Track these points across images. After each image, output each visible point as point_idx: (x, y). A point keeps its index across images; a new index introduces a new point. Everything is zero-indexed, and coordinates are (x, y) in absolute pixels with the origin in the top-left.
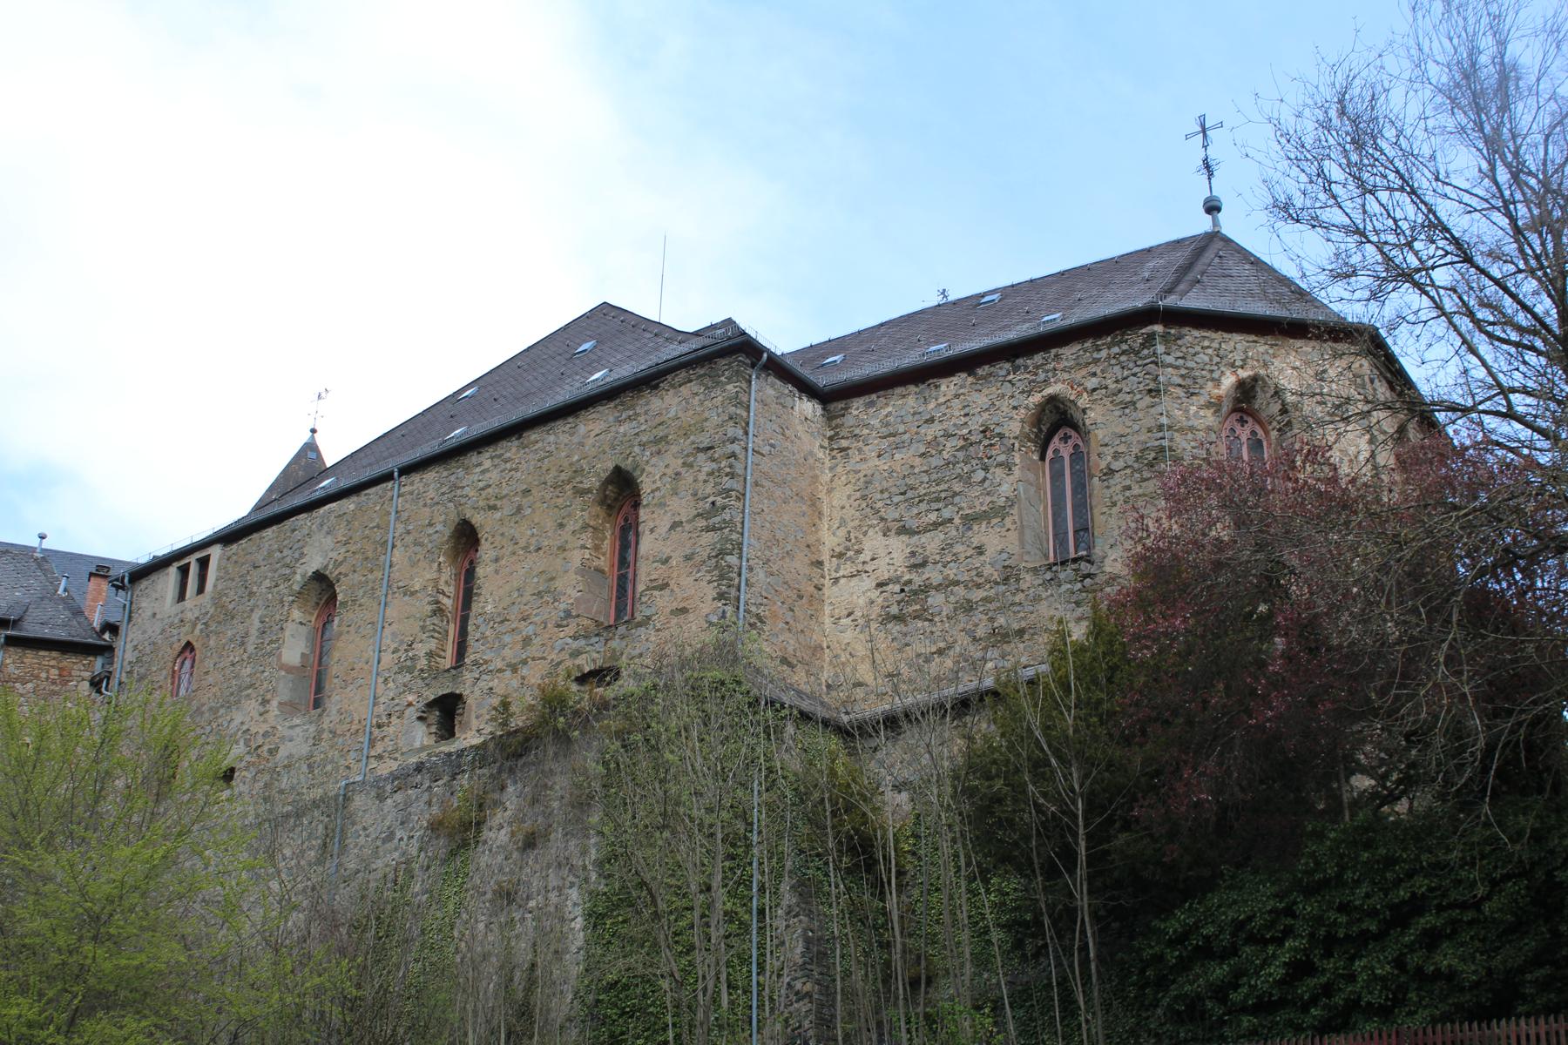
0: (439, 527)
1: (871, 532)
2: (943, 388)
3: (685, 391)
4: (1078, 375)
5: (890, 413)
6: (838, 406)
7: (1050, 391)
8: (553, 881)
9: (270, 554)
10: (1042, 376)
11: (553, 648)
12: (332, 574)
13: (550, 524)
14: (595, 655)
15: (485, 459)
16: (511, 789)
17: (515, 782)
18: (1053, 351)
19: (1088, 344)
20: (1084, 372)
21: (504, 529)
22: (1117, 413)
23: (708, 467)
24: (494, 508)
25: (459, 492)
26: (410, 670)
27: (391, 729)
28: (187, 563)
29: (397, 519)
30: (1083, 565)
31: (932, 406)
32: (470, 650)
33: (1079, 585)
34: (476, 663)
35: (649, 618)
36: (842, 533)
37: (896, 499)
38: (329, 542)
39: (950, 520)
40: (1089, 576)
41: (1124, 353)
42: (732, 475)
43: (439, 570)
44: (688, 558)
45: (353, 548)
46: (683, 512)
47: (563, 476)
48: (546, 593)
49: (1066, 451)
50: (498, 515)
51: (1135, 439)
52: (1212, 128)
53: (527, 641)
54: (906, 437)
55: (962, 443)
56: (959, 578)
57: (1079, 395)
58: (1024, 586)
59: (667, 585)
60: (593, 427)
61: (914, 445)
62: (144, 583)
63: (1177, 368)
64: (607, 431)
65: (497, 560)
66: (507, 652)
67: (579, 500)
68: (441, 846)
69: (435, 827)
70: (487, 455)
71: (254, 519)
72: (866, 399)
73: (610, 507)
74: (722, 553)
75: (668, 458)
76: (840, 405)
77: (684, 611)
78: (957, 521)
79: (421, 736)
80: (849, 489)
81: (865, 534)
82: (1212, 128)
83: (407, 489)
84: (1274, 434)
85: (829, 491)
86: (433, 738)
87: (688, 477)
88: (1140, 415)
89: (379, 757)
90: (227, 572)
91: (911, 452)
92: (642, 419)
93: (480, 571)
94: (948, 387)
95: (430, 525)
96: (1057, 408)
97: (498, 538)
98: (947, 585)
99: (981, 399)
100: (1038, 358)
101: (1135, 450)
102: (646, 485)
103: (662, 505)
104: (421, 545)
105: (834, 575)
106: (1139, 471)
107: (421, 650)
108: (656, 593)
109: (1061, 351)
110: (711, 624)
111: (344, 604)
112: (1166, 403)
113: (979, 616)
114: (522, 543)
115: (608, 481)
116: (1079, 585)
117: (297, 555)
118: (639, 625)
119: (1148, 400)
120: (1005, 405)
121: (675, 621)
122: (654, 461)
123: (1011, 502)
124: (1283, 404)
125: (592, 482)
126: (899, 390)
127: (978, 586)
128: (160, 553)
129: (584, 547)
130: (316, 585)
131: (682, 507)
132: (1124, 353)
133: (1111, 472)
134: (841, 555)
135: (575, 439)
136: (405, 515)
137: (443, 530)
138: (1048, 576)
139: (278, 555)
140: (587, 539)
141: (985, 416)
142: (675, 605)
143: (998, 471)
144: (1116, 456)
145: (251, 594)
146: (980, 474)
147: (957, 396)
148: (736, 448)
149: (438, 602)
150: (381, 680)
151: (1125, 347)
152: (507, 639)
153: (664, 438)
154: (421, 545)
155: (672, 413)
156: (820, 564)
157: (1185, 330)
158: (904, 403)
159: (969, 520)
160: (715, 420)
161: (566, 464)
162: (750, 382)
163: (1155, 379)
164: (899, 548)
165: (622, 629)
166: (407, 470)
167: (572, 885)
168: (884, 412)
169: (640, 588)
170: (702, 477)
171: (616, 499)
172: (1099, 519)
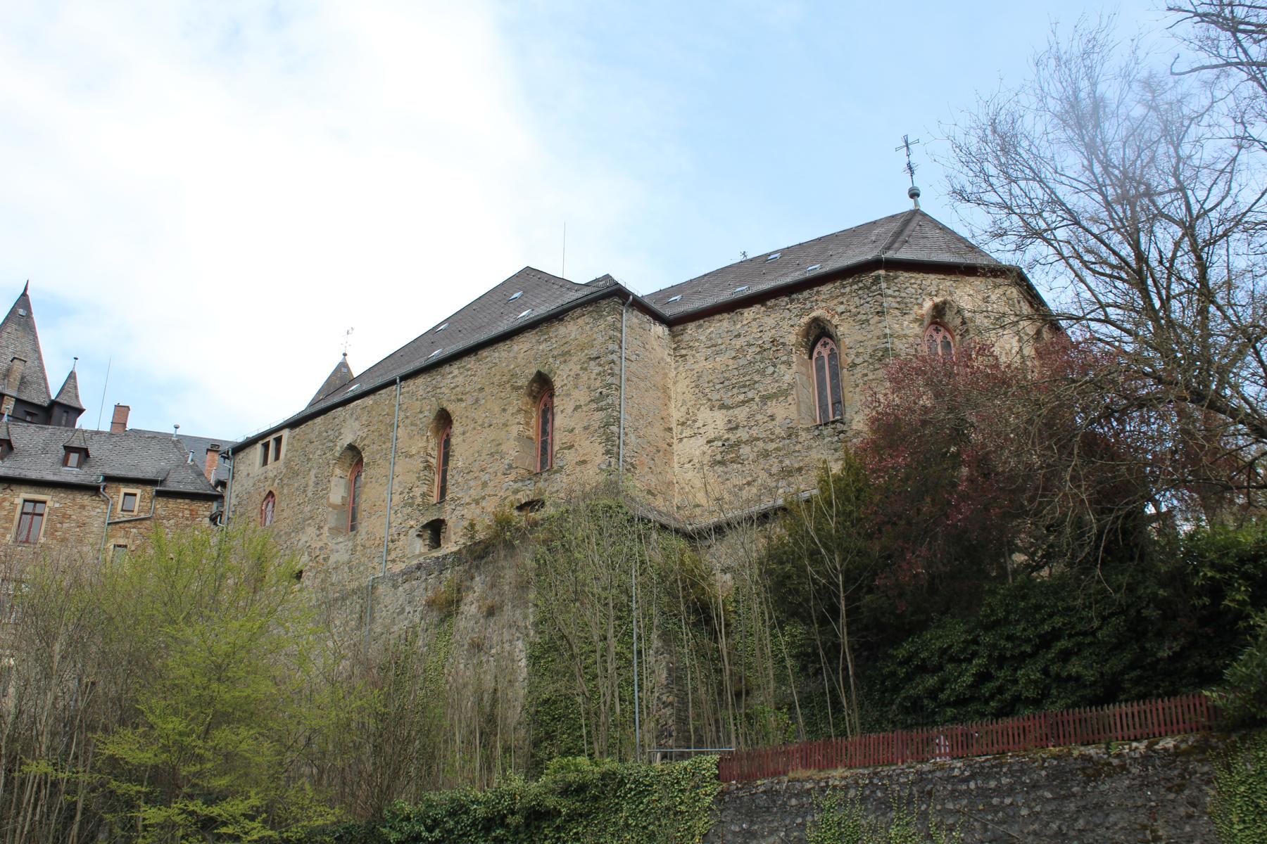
0: (426, 413)
7: (814, 314)
8: (506, 637)
10: (809, 305)
12: (359, 445)
15: (455, 369)
16: (477, 579)
19: (837, 284)
24: (461, 400)
26: (411, 505)
27: (401, 543)
28: (267, 441)
30: (839, 426)
34: (452, 499)
36: (684, 409)
37: (718, 387)
38: (357, 425)
39: (753, 399)
40: (842, 432)
44: (585, 428)
47: (505, 379)
48: (496, 454)
50: (464, 405)
51: (868, 344)
53: (485, 484)
57: (833, 316)
58: (801, 440)
60: (522, 347)
62: (241, 455)
64: (532, 349)
67: (515, 394)
68: (434, 616)
69: (430, 604)
71: (309, 412)
72: (697, 323)
73: (535, 397)
74: (607, 425)
75: (571, 365)
76: (680, 327)
77: (584, 462)
78: (757, 399)
79: (420, 547)
80: (687, 381)
84: (958, 338)
85: (675, 383)
87: (584, 376)
89: (394, 561)
93: (453, 441)
94: (749, 313)
95: (421, 412)
98: (752, 440)
99: (770, 321)
100: (806, 294)
101: (870, 351)
102: (557, 383)
103: (568, 395)
106: (872, 364)
107: (417, 492)
111: (367, 464)
112: (888, 320)
114: (480, 422)
115: (533, 381)
118: (556, 472)
119: (877, 318)
120: (785, 325)
121: (578, 469)
125: (523, 382)
126: (717, 317)
127: (772, 441)
130: (349, 453)
131: (581, 396)
133: (855, 365)
134: (683, 424)
135: (511, 355)
136: (404, 407)
137: (429, 415)
140: (521, 418)
141: (773, 331)
142: (578, 459)
143: (783, 367)
144: (858, 355)
145: (309, 460)
146: (771, 369)
147: (755, 320)
148: (614, 357)
152: (472, 483)
156: (670, 429)
157: (899, 273)
158: (720, 326)
159: (765, 399)
160: (601, 340)
163: (881, 305)
164: (720, 418)
165: (545, 475)
166: (405, 378)
167: (518, 639)
169: (556, 448)
170: (593, 376)
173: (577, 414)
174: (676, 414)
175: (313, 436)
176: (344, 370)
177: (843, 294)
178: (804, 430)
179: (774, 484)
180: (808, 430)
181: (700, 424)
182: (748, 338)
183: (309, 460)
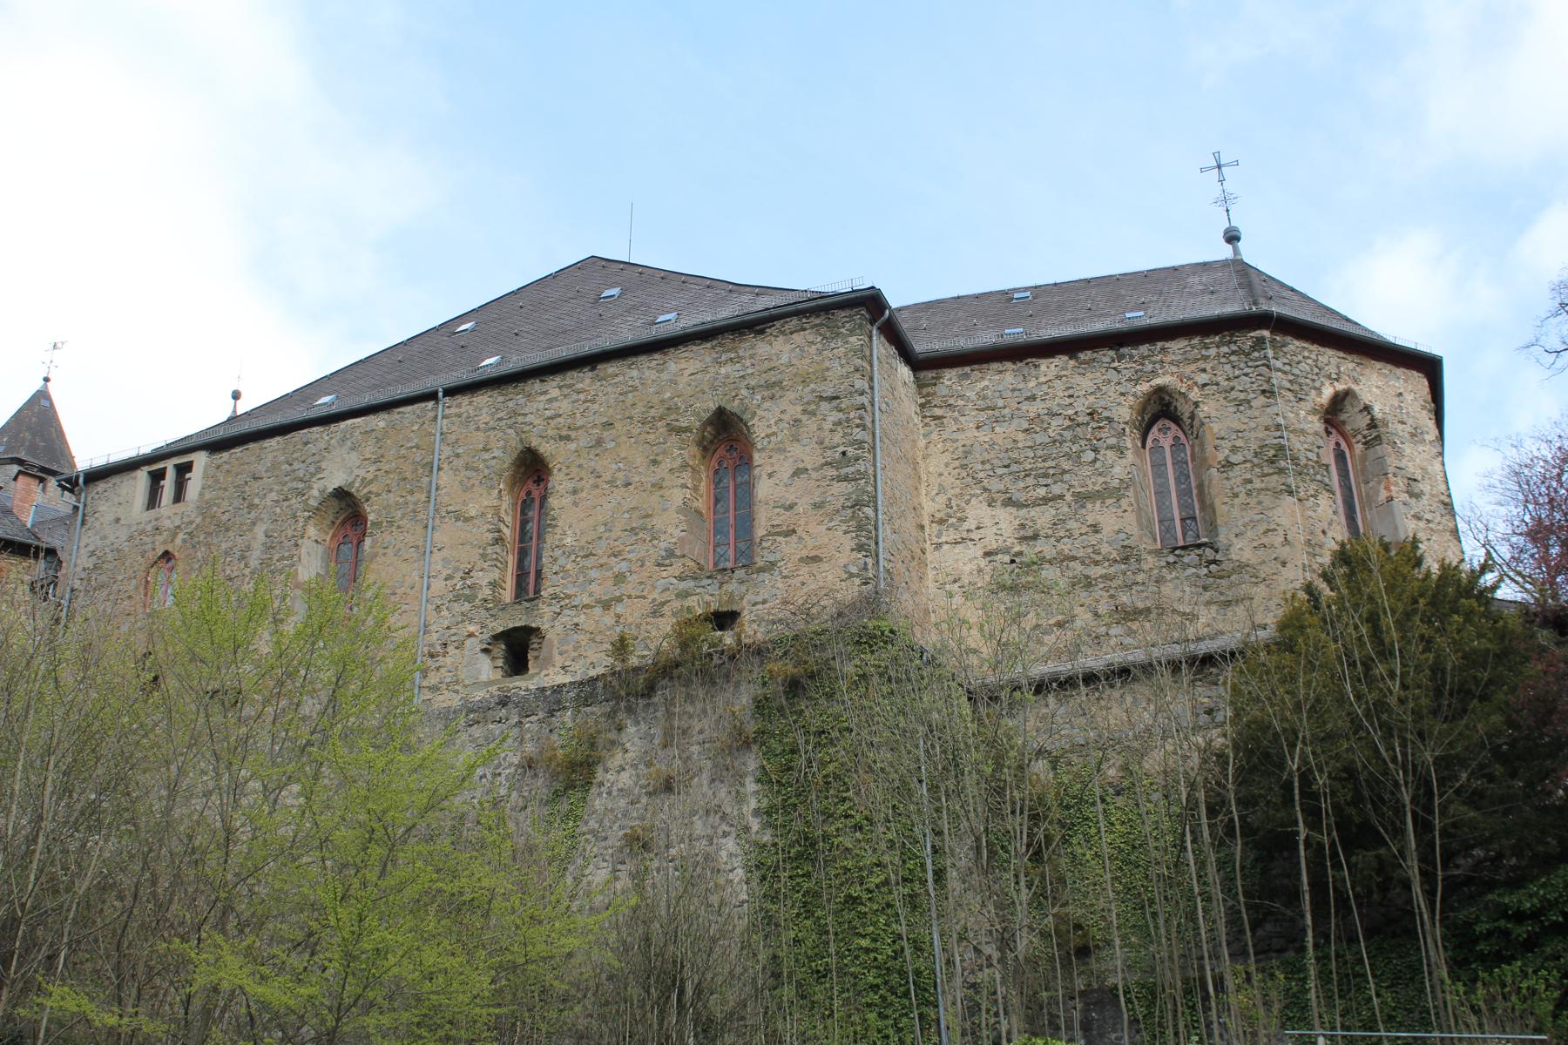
0: (497, 453)
1: (974, 501)
2: (1043, 368)
3: (798, 338)
4: (1188, 369)
6: (929, 374)
7: (1158, 381)
8: (699, 827)
9: (275, 466)
10: (1149, 367)
11: (654, 587)
12: (358, 491)
13: (639, 460)
14: (708, 598)
15: (553, 387)
16: (631, 729)
17: (638, 723)
18: (1159, 345)
19: (1196, 341)
20: (1193, 367)
21: (582, 461)
22: (1232, 409)
23: (835, 416)
24: (568, 438)
25: (520, 419)
26: (469, 599)
27: (448, 660)
28: (163, 468)
29: (442, 440)
30: (1209, 553)
31: (1032, 384)
32: (546, 583)
33: (1205, 571)
34: (555, 597)
35: (773, 564)
36: (942, 499)
37: (1000, 471)
38: (354, 458)
39: (1061, 497)
40: (1214, 562)
41: (1233, 353)
42: (864, 428)
43: (500, 497)
44: (817, 506)
45: (387, 467)
46: (807, 459)
47: (653, 412)
48: (641, 529)
49: (1166, 442)
50: (573, 446)
51: (1253, 435)
52: (1227, 165)
53: (619, 578)
54: (1006, 411)
55: (1067, 423)
56: (1074, 553)
57: (1190, 388)
58: (1145, 567)
59: (794, 531)
60: (685, 366)
61: (1016, 421)
62: (101, 486)
63: (1285, 373)
64: (705, 370)
65: (575, 492)
66: (594, 587)
67: (674, 438)
68: (540, 785)
69: (529, 765)
70: (554, 384)
71: (221, 434)
72: (959, 371)
73: (705, 449)
74: (857, 504)
75: (783, 404)
76: (930, 374)
77: (816, 559)
78: (1068, 497)
79: (487, 670)
80: (947, 457)
82: (1227, 165)
83: (453, 410)
84: (1359, 448)
85: (925, 458)
86: (499, 673)
87: (811, 424)
88: (1257, 413)
89: (434, 689)
90: (217, 481)
91: (1013, 427)
92: (748, 363)
93: (553, 502)
94: (1049, 367)
95: (486, 450)
96: (1162, 399)
97: (574, 470)
98: (1064, 559)
99: (1085, 383)
100: (1144, 349)
101: (1254, 446)
102: (759, 429)
103: (781, 450)
104: (476, 470)
105: (935, 540)
106: (1258, 465)
107: (482, 578)
108: (779, 539)
109: (1167, 345)
110: (851, 575)
111: (377, 524)
112: (1280, 405)
113: (1098, 593)
114: (607, 476)
115: (710, 422)
116: (1205, 571)
117: (312, 469)
118: (761, 570)
119: (1262, 400)
120: (1111, 391)
121: (805, 569)
122: (766, 405)
123: (1126, 484)
124: (1372, 419)
125: (689, 420)
126: (995, 366)
127: (1096, 563)
129: (684, 486)
130: (335, 503)
132: (1233, 353)
133: (1229, 465)
134: (941, 522)
135: (664, 376)
136: (452, 438)
137: (502, 456)
138: (1171, 559)
139: (285, 467)
140: (686, 477)
141: (1091, 399)
142: (805, 553)
143: (1109, 452)
144: (1234, 449)
145: (251, 506)
146: (1090, 456)
147: (1059, 377)
148: (864, 400)
149: (499, 531)
150: (430, 607)
151: (1234, 348)
152: (593, 574)
153: (779, 384)
154: (476, 470)
155: (784, 359)
156: (922, 527)
157: (1288, 339)
158: (1001, 380)
159: (1083, 498)
160: (840, 371)
161: (655, 400)
162: (870, 337)
163: (1268, 381)
164: (1007, 520)
165: (740, 573)
166: (451, 392)
167: (725, 834)
168: (981, 385)
169: (760, 532)
170: (828, 426)
171: (712, 442)
172: (1221, 509)
173: (799, 482)
174: (930, 506)
175: (261, 469)
176: (43, 402)
178: (1150, 552)
179: (1103, 630)
180: (1158, 553)
181: (971, 524)
182: (1048, 404)
183: (251, 506)
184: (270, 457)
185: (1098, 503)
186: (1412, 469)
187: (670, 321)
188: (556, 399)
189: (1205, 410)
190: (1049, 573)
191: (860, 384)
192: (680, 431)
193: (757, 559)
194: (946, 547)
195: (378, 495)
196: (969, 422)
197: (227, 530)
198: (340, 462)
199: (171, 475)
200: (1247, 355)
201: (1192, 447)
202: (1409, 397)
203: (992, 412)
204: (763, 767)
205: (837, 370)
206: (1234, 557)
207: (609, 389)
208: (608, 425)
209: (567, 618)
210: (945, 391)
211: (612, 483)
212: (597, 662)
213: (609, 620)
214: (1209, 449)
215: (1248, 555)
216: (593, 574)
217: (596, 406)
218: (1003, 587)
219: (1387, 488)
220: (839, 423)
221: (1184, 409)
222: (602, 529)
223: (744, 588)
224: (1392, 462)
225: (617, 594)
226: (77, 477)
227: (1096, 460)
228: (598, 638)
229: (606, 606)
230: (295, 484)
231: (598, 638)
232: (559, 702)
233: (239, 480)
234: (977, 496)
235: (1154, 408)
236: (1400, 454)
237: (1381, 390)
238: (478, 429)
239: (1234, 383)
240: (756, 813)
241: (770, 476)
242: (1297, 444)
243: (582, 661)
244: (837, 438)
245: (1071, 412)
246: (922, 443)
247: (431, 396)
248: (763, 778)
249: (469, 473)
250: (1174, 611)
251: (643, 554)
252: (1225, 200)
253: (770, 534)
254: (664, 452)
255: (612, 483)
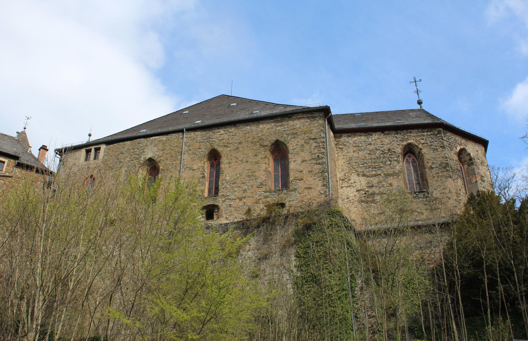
1: (353, 174)
3: (302, 120)
4: (418, 139)
5: (356, 140)
7: (409, 141)
9: (129, 150)
10: (406, 137)
14: (274, 198)
18: (409, 131)
20: (420, 138)
21: (231, 154)
24: (227, 146)
25: (211, 140)
31: (370, 140)
32: (220, 191)
34: (223, 196)
35: (296, 189)
36: (343, 173)
37: (361, 166)
38: (155, 149)
39: (380, 175)
41: (432, 134)
45: (166, 152)
47: (255, 140)
48: (252, 176)
51: (439, 159)
54: (362, 148)
55: (382, 152)
57: (419, 144)
61: (366, 151)
64: (272, 128)
66: (236, 193)
67: (262, 148)
74: (323, 172)
76: (339, 135)
77: (310, 188)
78: (382, 175)
80: (344, 161)
81: (351, 175)
83: (188, 136)
87: (307, 147)
90: (109, 154)
93: (222, 166)
94: (375, 136)
95: (199, 148)
98: (381, 194)
101: (439, 163)
102: (290, 147)
103: (298, 154)
110: (321, 194)
114: (240, 159)
115: (273, 144)
117: (141, 151)
118: (292, 191)
119: (441, 149)
121: (306, 191)
122: (292, 140)
124: (471, 157)
126: (359, 134)
128: (74, 145)
129: (266, 163)
132: (432, 134)
133: (431, 168)
134: (343, 180)
135: (259, 129)
137: (205, 150)
138: (415, 195)
141: (389, 145)
142: (306, 186)
143: (395, 162)
144: (433, 163)
145: (120, 162)
146: (389, 163)
148: (324, 140)
152: (236, 189)
153: (296, 133)
155: (298, 126)
159: (387, 175)
161: (256, 136)
163: (443, 143)
165: (285, 191)
166: (188, 130)
167: (285, 273)
169: (291, 179)
170: (313, 147)
172: (430, 181)
173: (304, 164)
174: (339, 175)
175: (124, 151)
177: (423, 135)
178: (408, 193)
180: (411, 193)
184: (127, 147)
185: (392, 177)
186: (482, 173)
187: (258, 113)
188: (223, 134)
189: (424, 151)
190: (378, 198)
191: (323, 135)
192: (264, 146)
193: (290, 187)
194: (344, 188)
195: (163, 161)
196: (351, 150)
197: (112, 169)
198: (151, 150)
199: (93, 151)
200: (436, 135)
201: (419, 162)
202: (480, 152)
203: (358, 148)
204: (298, 252)
205: (315, 130)
206: (434, 196)
207: (240, 132)
208: (240, 143)
209: (227, 202)
210: (343, 141)
211: (242, 161)
212: (240, 217)
213: (241, 204)
214: (425, 163)
215: (438, 195)
216: (236, 189)
217: (236, 137)
218: (363, 201)
219: (476, 178)
220: (316, 147)
221: (417, 151)
222: (239, 175)
223: (286, 196)
224: (476, 171)
225: (244, 195)
226: (62, 150)
227: (390, 164)
228: (238, 209)
229: (241, 199)
230: (135, 156)
231: (238, 209)
232: (227, 229)
233: (116, 153)
234: (354, 173)
235: (407, 149)
236: (478, 169)
237: (472, 148)
238: (197, 142)
239: (432, 144)
240: (295, 266)
241: (294, 161)
242: (451, 163)
243: (232, 216)
244: (316, 151)
245: (382, 149)
246: (336, 156)
247: (181, 131)
248: (298, 256)
249: (194, 156)
250: (416, 211)
251: (252, 183)
252: (418, 92)
253: (294, 179)
254: (259, 152)
255: (242, 161)
